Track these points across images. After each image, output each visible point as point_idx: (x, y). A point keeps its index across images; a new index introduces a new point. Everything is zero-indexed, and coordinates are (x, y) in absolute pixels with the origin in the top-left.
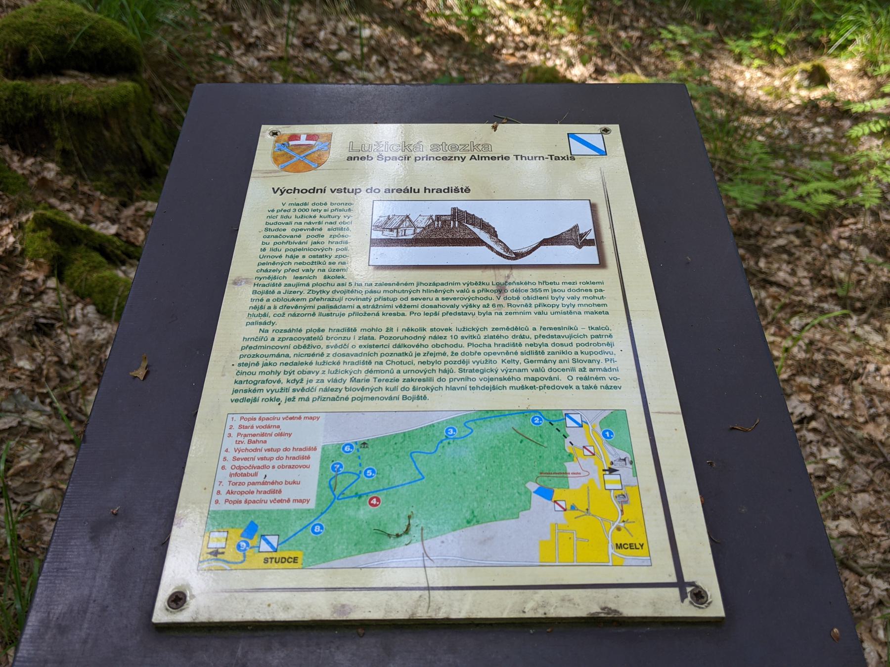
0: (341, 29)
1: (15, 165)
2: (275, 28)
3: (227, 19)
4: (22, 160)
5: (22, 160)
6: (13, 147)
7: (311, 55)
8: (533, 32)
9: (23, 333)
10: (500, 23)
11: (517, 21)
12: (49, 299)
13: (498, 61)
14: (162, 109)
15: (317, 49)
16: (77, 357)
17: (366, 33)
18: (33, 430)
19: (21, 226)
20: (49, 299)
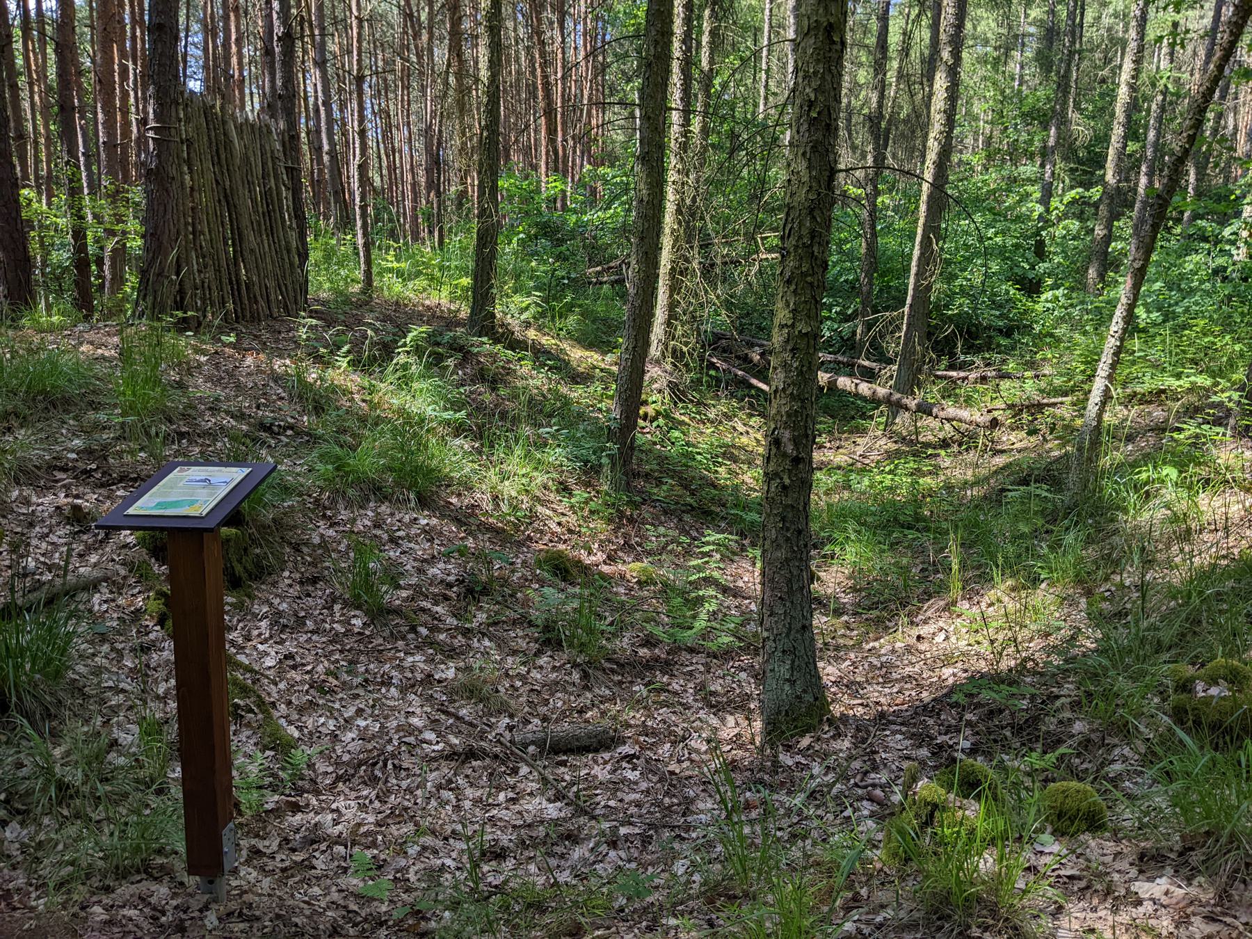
0: (407, 519)
1: (156, 568)
2: (890, 362)
3: (325, 508)
4: (160, 566)
5: (160, 566)
6: (157, 560)
7: (379, 532)
8: (570, 531)
9: (133, 650)
10: (545, 525)
11: (559, 524)
12: (152, 636)
13: (1116, 532)
14: (258, 551)
15: (382, 529)
16: (159, 666)
17: (424, 522)
18: (123, 691)
19: (1013, 79)
20: (152, 636)
